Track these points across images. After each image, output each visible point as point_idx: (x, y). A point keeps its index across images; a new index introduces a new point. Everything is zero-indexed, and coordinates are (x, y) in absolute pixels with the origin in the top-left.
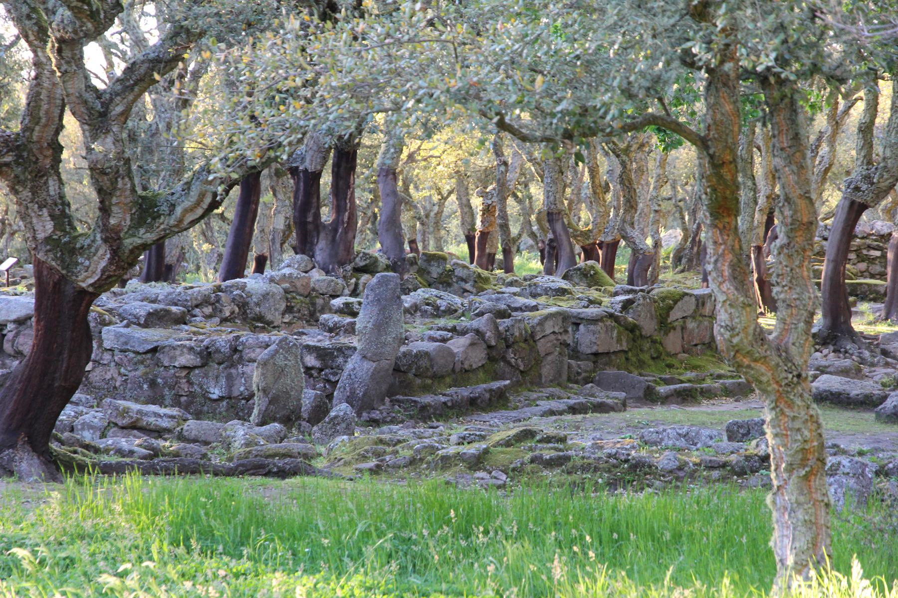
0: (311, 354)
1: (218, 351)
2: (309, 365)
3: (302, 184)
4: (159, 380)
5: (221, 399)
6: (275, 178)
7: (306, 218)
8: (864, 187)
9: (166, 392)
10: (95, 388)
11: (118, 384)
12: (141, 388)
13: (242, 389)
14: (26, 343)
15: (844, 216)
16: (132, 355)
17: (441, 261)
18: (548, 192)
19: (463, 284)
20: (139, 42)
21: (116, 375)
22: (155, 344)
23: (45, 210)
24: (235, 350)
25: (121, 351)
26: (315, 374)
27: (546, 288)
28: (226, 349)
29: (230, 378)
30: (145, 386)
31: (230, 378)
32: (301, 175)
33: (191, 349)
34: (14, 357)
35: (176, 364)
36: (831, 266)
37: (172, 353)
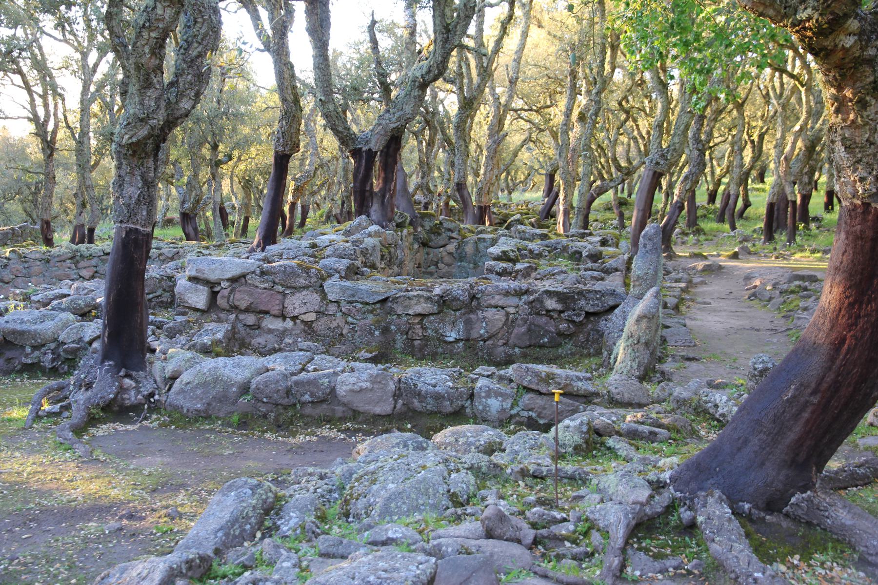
0: (551, 298)
1: (456, 299)
2: (550, 308)
3: (364, 161)
4: (393, 327)
5: (457, 341)
8: (662, 162)
9: (398, 336)
10: (320, 335)
11: (345, 332)
12: (372, 334)
13: (482, 331)
14: (242, 299)
15: (649, 181)
16: (359, 306)
19: (449, 233)
21: (342, 324)
22: (386, 295)
24: (473, 297)
25: (349, 302)
26: (555, 315)
28: (465, 297)
29: (468, 323)
30: (377, 333)
31: (468, 323)
33: (429, 299)
34: (228, 311)
35: (410, 312)
36: (641, 214)
37: (407, 302)
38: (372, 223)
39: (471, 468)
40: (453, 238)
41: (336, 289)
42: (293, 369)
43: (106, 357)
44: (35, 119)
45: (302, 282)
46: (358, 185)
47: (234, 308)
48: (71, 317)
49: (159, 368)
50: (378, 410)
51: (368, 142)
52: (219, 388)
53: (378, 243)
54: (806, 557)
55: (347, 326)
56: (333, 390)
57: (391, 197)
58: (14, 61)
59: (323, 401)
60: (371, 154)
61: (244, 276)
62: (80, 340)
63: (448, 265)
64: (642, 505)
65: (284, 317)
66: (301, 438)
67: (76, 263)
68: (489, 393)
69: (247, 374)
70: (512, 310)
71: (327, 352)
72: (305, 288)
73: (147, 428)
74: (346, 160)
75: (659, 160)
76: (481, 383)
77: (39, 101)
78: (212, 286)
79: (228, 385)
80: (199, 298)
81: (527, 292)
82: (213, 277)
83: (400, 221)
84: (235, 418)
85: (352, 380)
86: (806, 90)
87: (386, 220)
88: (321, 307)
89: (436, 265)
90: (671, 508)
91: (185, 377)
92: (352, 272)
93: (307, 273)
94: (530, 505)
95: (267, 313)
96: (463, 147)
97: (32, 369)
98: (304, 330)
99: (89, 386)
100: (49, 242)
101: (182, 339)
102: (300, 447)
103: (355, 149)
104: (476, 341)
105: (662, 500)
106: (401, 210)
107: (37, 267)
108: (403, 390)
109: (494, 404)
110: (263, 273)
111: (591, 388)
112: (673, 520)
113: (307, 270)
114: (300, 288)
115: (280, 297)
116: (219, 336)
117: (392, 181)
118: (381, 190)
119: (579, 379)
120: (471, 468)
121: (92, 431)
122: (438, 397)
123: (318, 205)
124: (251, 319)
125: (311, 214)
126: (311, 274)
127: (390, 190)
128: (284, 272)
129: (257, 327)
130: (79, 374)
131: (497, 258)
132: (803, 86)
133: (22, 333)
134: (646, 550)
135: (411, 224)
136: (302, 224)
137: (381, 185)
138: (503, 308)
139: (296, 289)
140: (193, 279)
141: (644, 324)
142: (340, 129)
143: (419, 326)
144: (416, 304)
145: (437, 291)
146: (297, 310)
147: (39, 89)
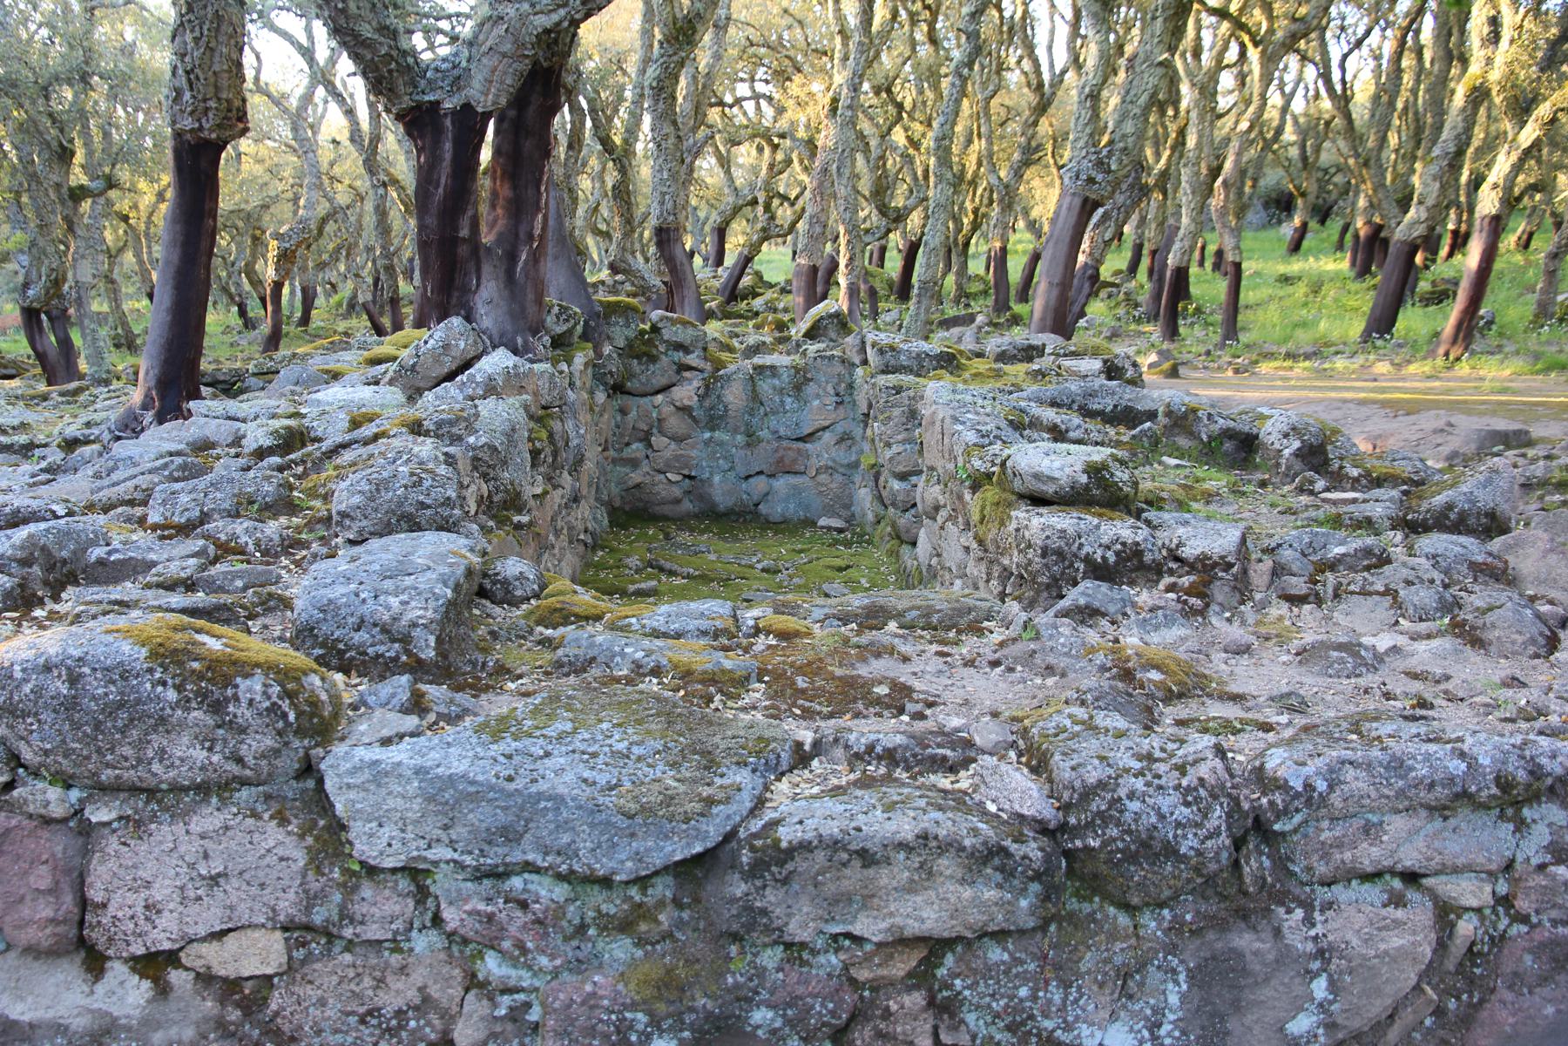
3: (448, 146)
6: (70, 203)
7: (456, 229)
8: (1099, 178)
16: (547, 891)
17: (630, 313)
18: (663, 194)
19: (678, 356)
21: (447, 992)
25: (480, 875)
27: (918, 355)
32: (448, 122)
36: (1055, 292)
37: (854, 876)
40: (690, 368)
41: (403, 800)
46: (431, 221)
53: (521, 416)
55: (475, 1005)
57: (535, 258)
60: (469, 123)
63: (678, 439)
70: (1470, 892)
72: (211, 789)
74: (381, 191)
75: (1094, 174)
83: (560, 329)
86: (1263, 53)
88: (311, 900)
89: (646, 439)
93: (217, 707)
96: (672, 140)
98: (221, 1025)
103: (419, 106)
114: (177, 789)
115: (59, 844)
117: (538, 209)
118: (499, 241)
123: (333, 286)
125: (320, 301)
126: (243, 713)
127: (531, 237)
128: (70, 705)
132: (1256, 45)
135: (585, 337)
136: (305, 320)
137: (501, 222)
138: (1412, 877)
142: (367, 31)
143: (916, 999)
144: (911, 888)
146: (167, 921)
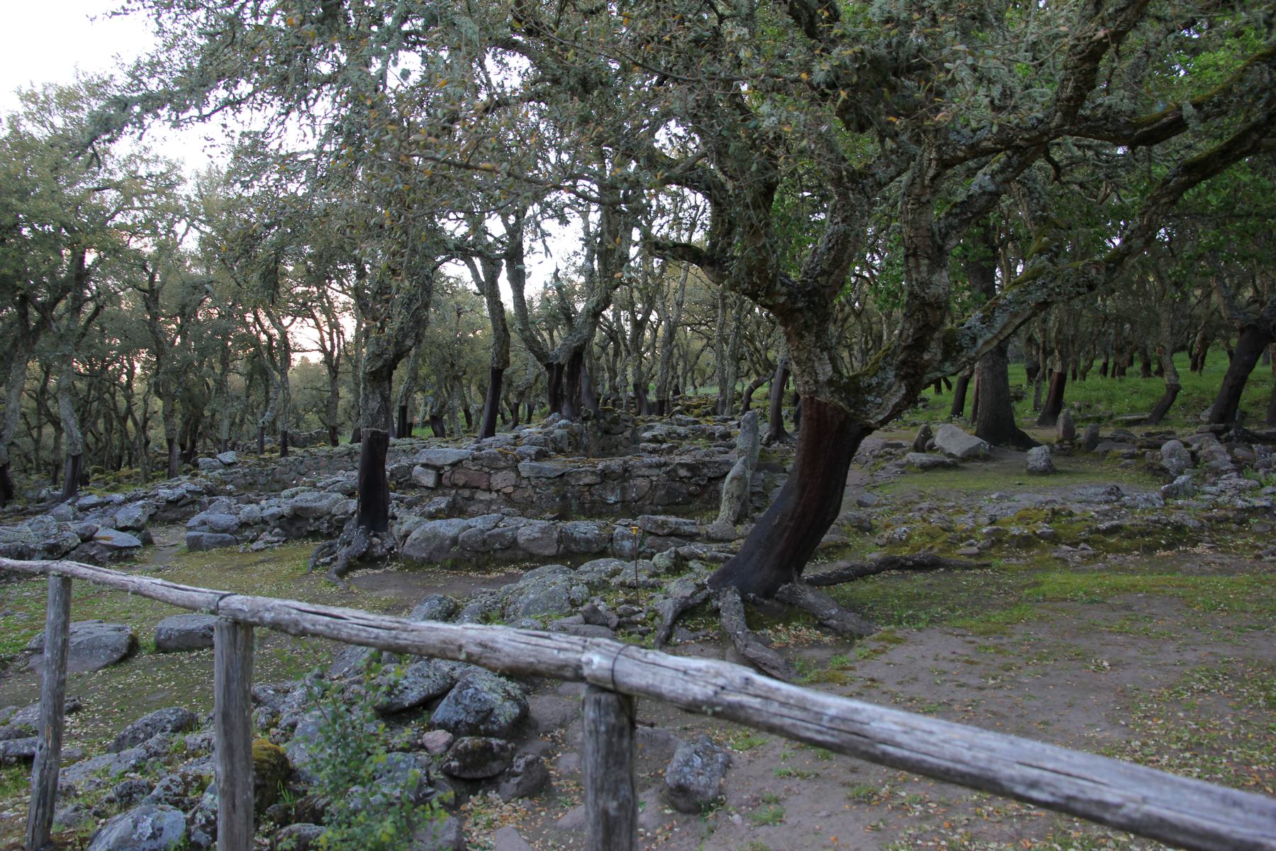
1: (613, 472)
5: (616, 503)
9: (573, 501)
20: (678, 238)
23: (825, 353)
24: (626, 470)
28: (620, 470)
29: (624, 490)
33: (593, 473)
38: (562, 418)
39: (587, 584)
42: (489, 526)
43: (360, 522)
44: (323, 350)
45: (503, 464)
47: (454, 486)
48: (341, 496)
49: (397, 529)
50: (547, 553)
51: (557, 357)
52: (437, 542)
54: (786, 625)
56: (515, 540)
58: (310, 309)
59: (508, 548)
60: (560, 367)
61: (460, 461)
62: (346, 512)
64: (687, 598)
65: (489, 490)
66: (494, 575)
67: (352, 458)
68: (623, 537)
69: (456, 530)
70: (654, 478)
71: (522, 515)
72: (505, 468)
73: (389, 572)
76: (619, 529)
77: (326, 337)
78: (438, 469)
79: (443, 539)
80: (429, 479)
81: (665, 464)
82: (439, 463)
84: (449, 562)
85: (528, 532)
87: (575, 413)
89: (617, 447)
90: (707, 600)
91: (414, 535)
92: (541, 455)
94: (620, 604)
95: (478, 488)
97: (315, 535)
99: (349, 544)
100: (335, 443)
101: (417, 509)
102: (492, 580)
104: (630, 502)
105: (701, 596)
106: (587, 407)
107: (324, 462)
108: (564, 538)
109: (627, 544)
110: (474, 459)
111: (694, 530)
112: (708, 607)
113: (505, 455)
116: (443, 506)
119: (686, 524)
120: (587, 584)
121: (351, 574)
122: (588, 541)
124: (467, 493)
129: (471, 498)
130: (344, 536)
131: (650, 441)
133: (306, 509)
134: (687, 627)
139: (499, 469)
140: (425, 466)
141: (735, 482)
145: (600, 467)
147: (327, 329)
